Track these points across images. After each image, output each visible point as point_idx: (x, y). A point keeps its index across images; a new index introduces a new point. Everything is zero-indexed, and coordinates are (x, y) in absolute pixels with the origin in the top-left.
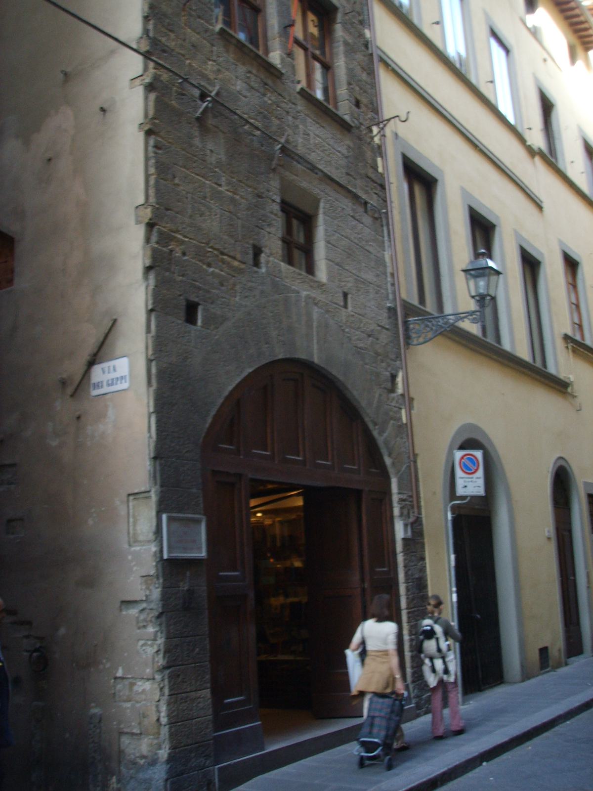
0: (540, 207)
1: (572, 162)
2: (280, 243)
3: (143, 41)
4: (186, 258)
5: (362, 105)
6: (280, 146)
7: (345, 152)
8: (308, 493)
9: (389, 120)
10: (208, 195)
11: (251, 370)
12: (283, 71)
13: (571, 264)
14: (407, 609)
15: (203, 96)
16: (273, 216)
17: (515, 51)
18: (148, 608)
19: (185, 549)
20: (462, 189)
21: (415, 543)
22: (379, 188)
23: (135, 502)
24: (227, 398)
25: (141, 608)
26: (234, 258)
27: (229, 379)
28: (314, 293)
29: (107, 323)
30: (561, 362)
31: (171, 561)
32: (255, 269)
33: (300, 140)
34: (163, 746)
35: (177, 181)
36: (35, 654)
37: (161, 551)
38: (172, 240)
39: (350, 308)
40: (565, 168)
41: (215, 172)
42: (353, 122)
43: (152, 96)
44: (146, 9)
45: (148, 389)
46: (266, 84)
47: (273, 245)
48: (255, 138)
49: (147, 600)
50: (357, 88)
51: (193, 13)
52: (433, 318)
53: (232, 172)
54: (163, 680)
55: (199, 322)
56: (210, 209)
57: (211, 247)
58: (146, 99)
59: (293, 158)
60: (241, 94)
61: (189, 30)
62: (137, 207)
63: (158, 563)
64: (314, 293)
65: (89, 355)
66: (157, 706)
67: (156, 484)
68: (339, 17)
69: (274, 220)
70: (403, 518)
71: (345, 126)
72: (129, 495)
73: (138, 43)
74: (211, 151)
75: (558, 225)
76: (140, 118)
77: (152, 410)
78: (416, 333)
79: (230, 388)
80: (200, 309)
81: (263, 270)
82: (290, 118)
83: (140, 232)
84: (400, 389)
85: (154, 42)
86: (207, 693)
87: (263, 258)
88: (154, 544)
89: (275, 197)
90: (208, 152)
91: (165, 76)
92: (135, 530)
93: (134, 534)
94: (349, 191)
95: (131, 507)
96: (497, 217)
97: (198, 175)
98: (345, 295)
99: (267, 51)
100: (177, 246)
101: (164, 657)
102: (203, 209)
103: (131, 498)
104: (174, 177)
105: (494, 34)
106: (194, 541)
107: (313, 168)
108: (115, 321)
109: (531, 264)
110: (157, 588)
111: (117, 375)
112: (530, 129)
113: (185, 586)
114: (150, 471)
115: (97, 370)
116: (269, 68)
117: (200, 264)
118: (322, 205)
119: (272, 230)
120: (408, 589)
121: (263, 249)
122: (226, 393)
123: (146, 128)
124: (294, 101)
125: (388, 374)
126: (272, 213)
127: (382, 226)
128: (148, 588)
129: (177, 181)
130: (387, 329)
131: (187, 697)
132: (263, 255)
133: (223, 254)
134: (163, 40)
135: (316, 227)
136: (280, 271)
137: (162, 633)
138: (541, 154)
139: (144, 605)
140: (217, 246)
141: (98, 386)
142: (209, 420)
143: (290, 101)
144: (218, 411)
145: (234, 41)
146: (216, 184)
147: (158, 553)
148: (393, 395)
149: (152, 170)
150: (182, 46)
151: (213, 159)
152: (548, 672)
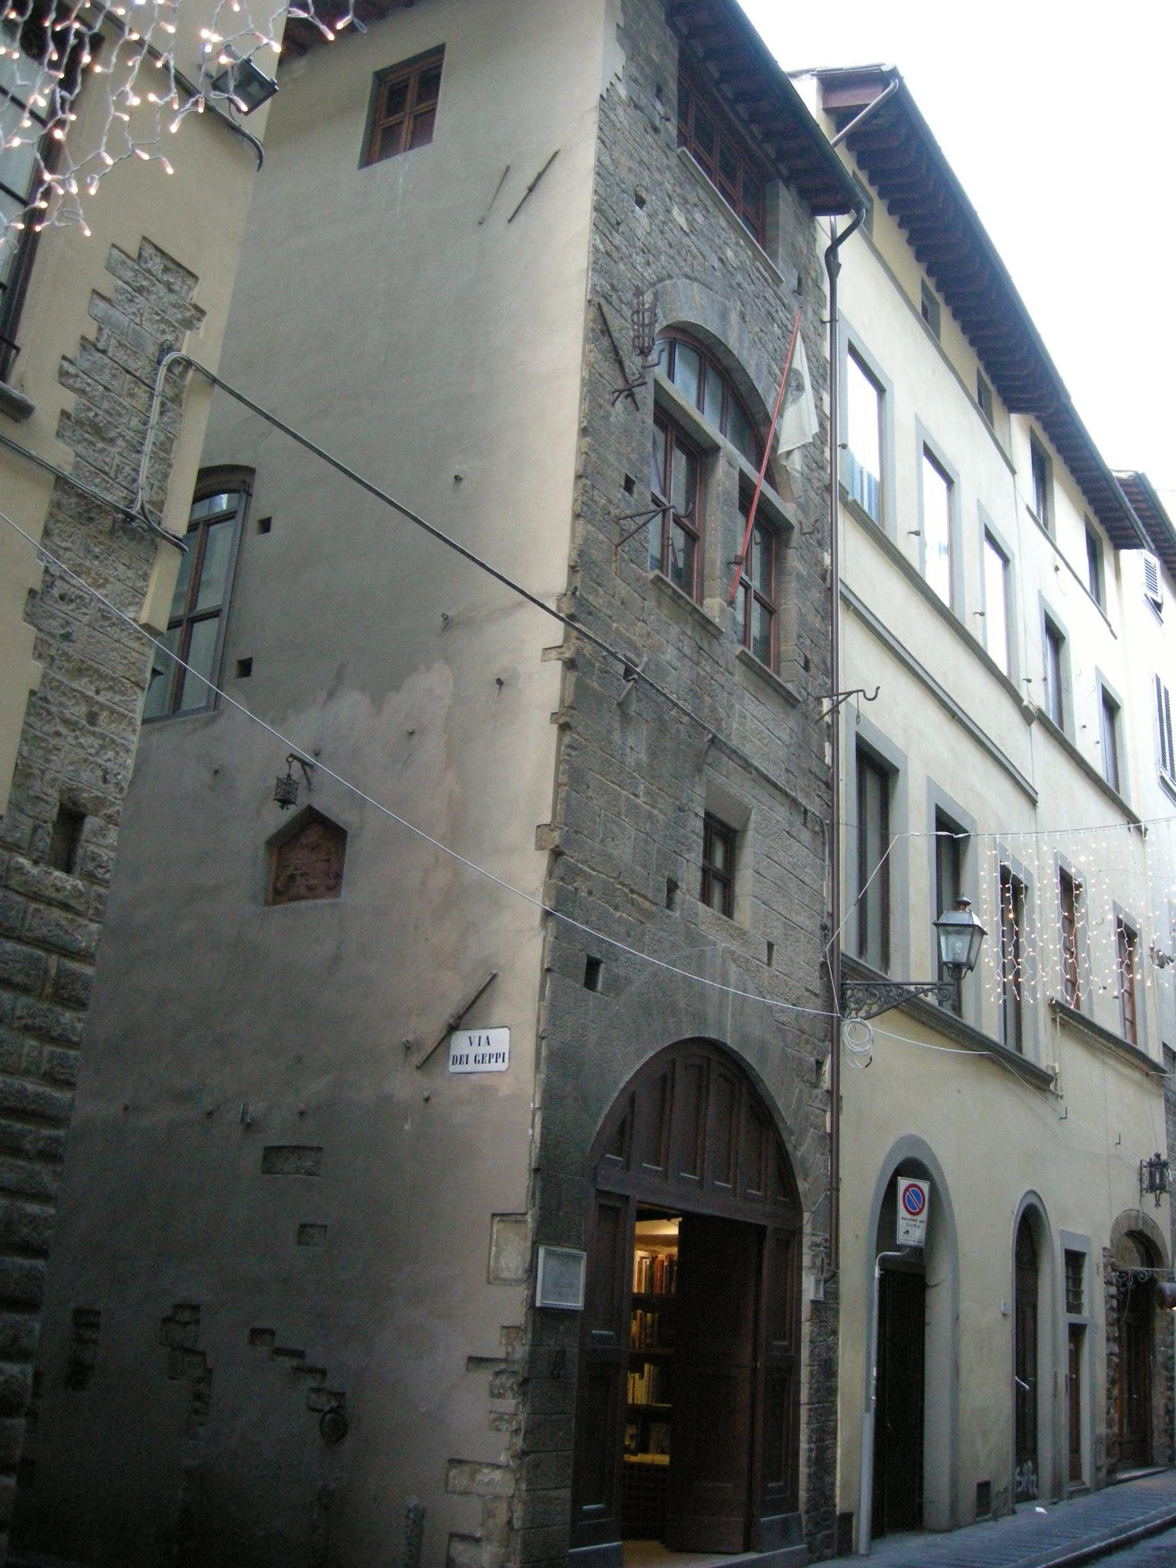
0: (1033, 802)
1: (1084, 727)
5: (812, 666)
6: (710, 736)
7: (785, 737)
8: (689, 1223)
9: (849, 694)
10: (623, 811)
11: (652, 1054)
13: (1069, 887)
14: (808, 1404)
15: (628, 672)
17: (1017, 563)
19: (560, 1295)
20: (929, 779)
21: (827, 1308)
22: (823, 787)
23: (501, 1225)
26: (645, 897)
28: (734, 946)
30: (1045, 1045)
31: (545, 1311)
33: (735, 725)
34: (513, 1558)
36: (329, 1416)
37: (533, 1296)
38: (578, 875)
39: (774, 966)
40: (1074, 736)
41: (633, 777)
42: (800, 693)
46: (701, 648)
47: (691, 877)
50: (808, 642)
52: (884, 985)
55: (600, 986)
56: (622, 829)
58: (564, 680)
59: (723, 752)
61: (619, 581)
62: (538, 827)
64: (734, 946)
66: (510, 1504)
68: (795, 536)
70: (815, 1271)
71: (790, 701)
72: (494, 1215)
73: (559, 600)
75: (1059, 829)
76: (554, 706)
78: (856, 1003)
79: (627, 1078)
80: (603, 966)
82: (725, 694)
83: (541, 861)
84: (826, 1083)
85: (581, 602)
86: (566, 1494)
87: (679, 896)
88: (524, 1286)
90: (628, 750)
91: (588, 649)
92: (497, 1262)
94: (787, 795)
95: (495, 1230)
96: (974, 821)
97: (613, 782)
98: (770, 946)
101: (524, 1440)
102: (615, 829)
105: (990, 537)
106: (571, 1285)
107: (746, 765)
108: (495, 976)
109: (1013, 889)
112: (1029, 681)
116: (705, 624)
118: (753, 817)
120: (812, 1375)
121: (679, 883)
122: (622, 1085)
123: (562, 721)
124: (731, 670)
125: (813, 1059)
126: (694, 832)
127: (824, 844)
130: (816, 995)
132: (678, 892)
133: (632, 891)
134: (590, 598)
135: (741, 847)
136: (696, 914)
138: (1042, 719)
139: (503, 1366)
141: (459, 1060)
142: (601, 1121)
143: (727, 670)
148: (817, 1091)
149: (564, 779)
151: (630, 760)
152: (987, 1520)
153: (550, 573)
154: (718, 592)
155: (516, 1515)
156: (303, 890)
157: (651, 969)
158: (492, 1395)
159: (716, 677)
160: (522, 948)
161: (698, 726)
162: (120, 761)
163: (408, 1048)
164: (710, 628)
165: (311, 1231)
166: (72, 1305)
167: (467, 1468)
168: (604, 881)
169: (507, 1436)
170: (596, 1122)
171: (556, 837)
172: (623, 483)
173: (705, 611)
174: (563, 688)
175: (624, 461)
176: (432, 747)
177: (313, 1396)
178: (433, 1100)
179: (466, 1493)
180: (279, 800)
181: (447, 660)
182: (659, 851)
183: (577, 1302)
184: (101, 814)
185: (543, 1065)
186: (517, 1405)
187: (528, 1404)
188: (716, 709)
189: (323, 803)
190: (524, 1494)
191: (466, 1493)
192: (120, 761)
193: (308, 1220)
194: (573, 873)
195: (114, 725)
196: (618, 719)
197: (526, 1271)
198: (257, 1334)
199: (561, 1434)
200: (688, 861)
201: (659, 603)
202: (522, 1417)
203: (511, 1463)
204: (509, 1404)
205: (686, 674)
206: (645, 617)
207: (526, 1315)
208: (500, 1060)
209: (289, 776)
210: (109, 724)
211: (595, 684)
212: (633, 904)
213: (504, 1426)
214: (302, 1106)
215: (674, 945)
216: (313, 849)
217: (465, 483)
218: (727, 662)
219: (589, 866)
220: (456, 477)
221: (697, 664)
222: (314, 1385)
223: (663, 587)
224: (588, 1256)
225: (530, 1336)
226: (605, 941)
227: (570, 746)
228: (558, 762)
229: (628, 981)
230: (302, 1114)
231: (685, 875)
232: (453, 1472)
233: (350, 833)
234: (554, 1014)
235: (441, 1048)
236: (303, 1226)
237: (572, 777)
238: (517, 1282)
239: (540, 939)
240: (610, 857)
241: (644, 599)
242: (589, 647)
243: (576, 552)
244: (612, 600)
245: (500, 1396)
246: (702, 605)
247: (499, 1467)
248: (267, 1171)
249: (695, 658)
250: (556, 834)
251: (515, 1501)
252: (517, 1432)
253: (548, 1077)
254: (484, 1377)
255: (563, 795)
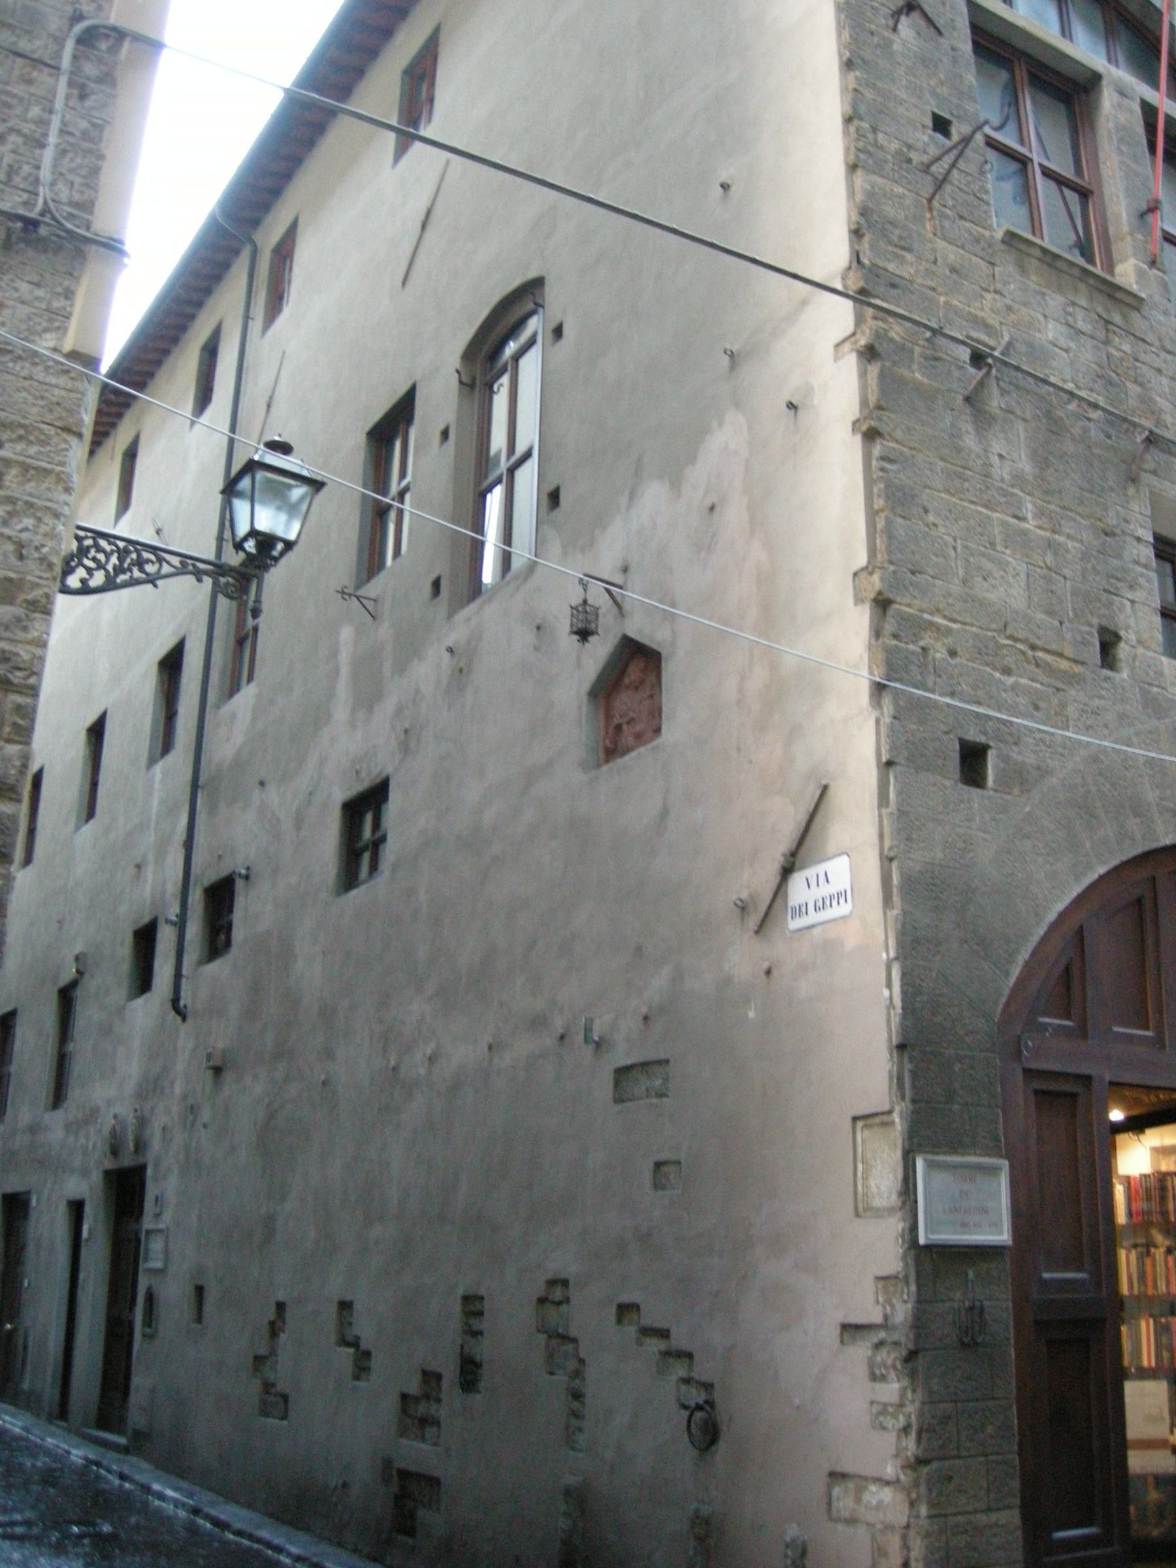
2: (1157, 620)
3: (851, 274)
4: (958, 660)
11: (1102, 870)
12: (1143, 295)
16: (1139, 569)
18: (889, 1340)
23: (866, 1132)
24: (1054, 926)
25: (876, 1340)
26: (1060, 655)
27: (1055, 888)
29: (813, 793)
32: (1106, 672)
35: (931, 518)
36: (699, 1415)
37: (914, 1228)
38: (925, 629)
41: (1012, 494)
43: (874, 370)
44: (855, 217)
45: (885, 914)
48: (1092, 425)
49: (885, 1325)
51: (949, 212)
53: (1048, 492)
54: (916, 1484)
56: (1003, 566)
57: (1011, 637)
58: (863, 374)
60: (1055, 345)
61: (941, 244)
63: (909, 1249)
65: (784, 855)
66: (904, 1538)
67: (903, 1098)
69: (1142, 575)
72: (855, 1119)
74: (1001, 456)
77: (892, 954)
80: (991, 756)
81: (1125, 675)
83: (860, 619)
85: (874, 273)
86: (1012, 1517)
87: (1123, 651)
89: (1140, 532)
90: (995, 460)
91: (897, 331)
92: (866, 1186)
93: (865, 1195)
97: (972, 502)
99: (1110, 266)
100: (937, 639)
101: (919, 1441)
103: (860, 1124)
104: (926, 511)
108: (825, 788)
110: (905, 1302)
111: (832, 889)
113: (957, 1298)
114: (890, 1072)
115: (797, 881)
116: (1112, 292)
117: (988, 670)
119: (1139, 595)
121: (1122, 633)
122: (1052, 916)
123: (864, 428)
126: (1137, 563)
128: (888, 1301)
129: (931, 518)
131: (969, 1523)
132: (1122, 645)
134: (891, 267)
136: (1160, 673)
137: (914, 1391)
139: (882, 1335)
140: (1021, 634)
141: (801, 911)
142: (1016, 972)
144: (1034, 953)
145: (1037, 253)
146: (1015, 517)
147: (907, 1231)
149: (879, 503)
150: (929, 273)
151: (1001, 472)
153: (829, 250)
154: (1130, 251)
155: (914, 1554)
156: (631, 741)
157: (1083, 752)
158: (874, 1377)
159: (1142, 357)
160: (849, 737)
161: (1120, 422)
162: (43, 529)
163: (743, 909)
164: (1119, 295)
165: (665, 1169)
166: (461, 1291)
167: (851, 1485)
168: (976, 635)
169: (891, 1437)
170: (1007, 974)
171: (876, 582)
172: (930, 123)
173: (1119, 280)
174: (864, 387)
175: (927, 96)
176: (734, 516)
177: (683, 1388)
178: (775, 973)
179: (852, 1521)
180: (576, 633)
181: (737, 405)
182: (1075, 593)
183: (1001, 1233)
184: (18, 601)
185: (896, 899)
186: (903, 1392)
187: (920, 1391)
188: (1151, 399)
189: (638, 628)
190: (924, 1522)
191: (852, 1521)
192: (43, 529)
193: (662, 1157)
194: (915, 627)
195: (33, 484)
196: (969, 418)
197: (900, 1194)
198: (625, 1310)
199: (990, 1430)
200: (1132, 602)
201: (1022, 269)
202: (910, 1408)
203: (902, 1477)
204: (891, 1390)
205: (1087, 355)
206: (999, 286)
207: (904, 1258)
208: (842, 900)
209: (585, 602)
210: (22, 484)
211: (918, 375)
212: (1038, 665)
213: (889, 1422)
214: (644, 1010)
215: (1122, 717)
216: (636, 688)
217: (733, 189)
218: (1160, 339)
219: (945, 617)
220: (722, 186)
221: (1107, 342)
222: (682, 1373)
223: (1023, 247)
224: (1012, 1166)
225: (913, 1288)
226: (989, 718)
227: (883, 458)
228: (869, 482)
229: (1043, 772)
230: (646, 1018)
231: (1132, 622)
232: (836, 1491)
233: (664, 654)
234: (904, 826)
235: (779, 901)
236: (658, 1165)
237: (893, 499)
238: (891, 1210)
239: (871, 723)
240: (983, 604)
241: (993, 264)
242: (897, 328)
243: (856, 211)
244: (934, 268)
245: (883, 1378)
246: (1112, 273)
247: (888, 1483)
248: (619, 1099)
249: (1101, 334)
250: (876, 578)
251: (912, 1533)
252: (906, 1430)
253: (905, 913)
254: (860, 1352)
255: (881, 523)
